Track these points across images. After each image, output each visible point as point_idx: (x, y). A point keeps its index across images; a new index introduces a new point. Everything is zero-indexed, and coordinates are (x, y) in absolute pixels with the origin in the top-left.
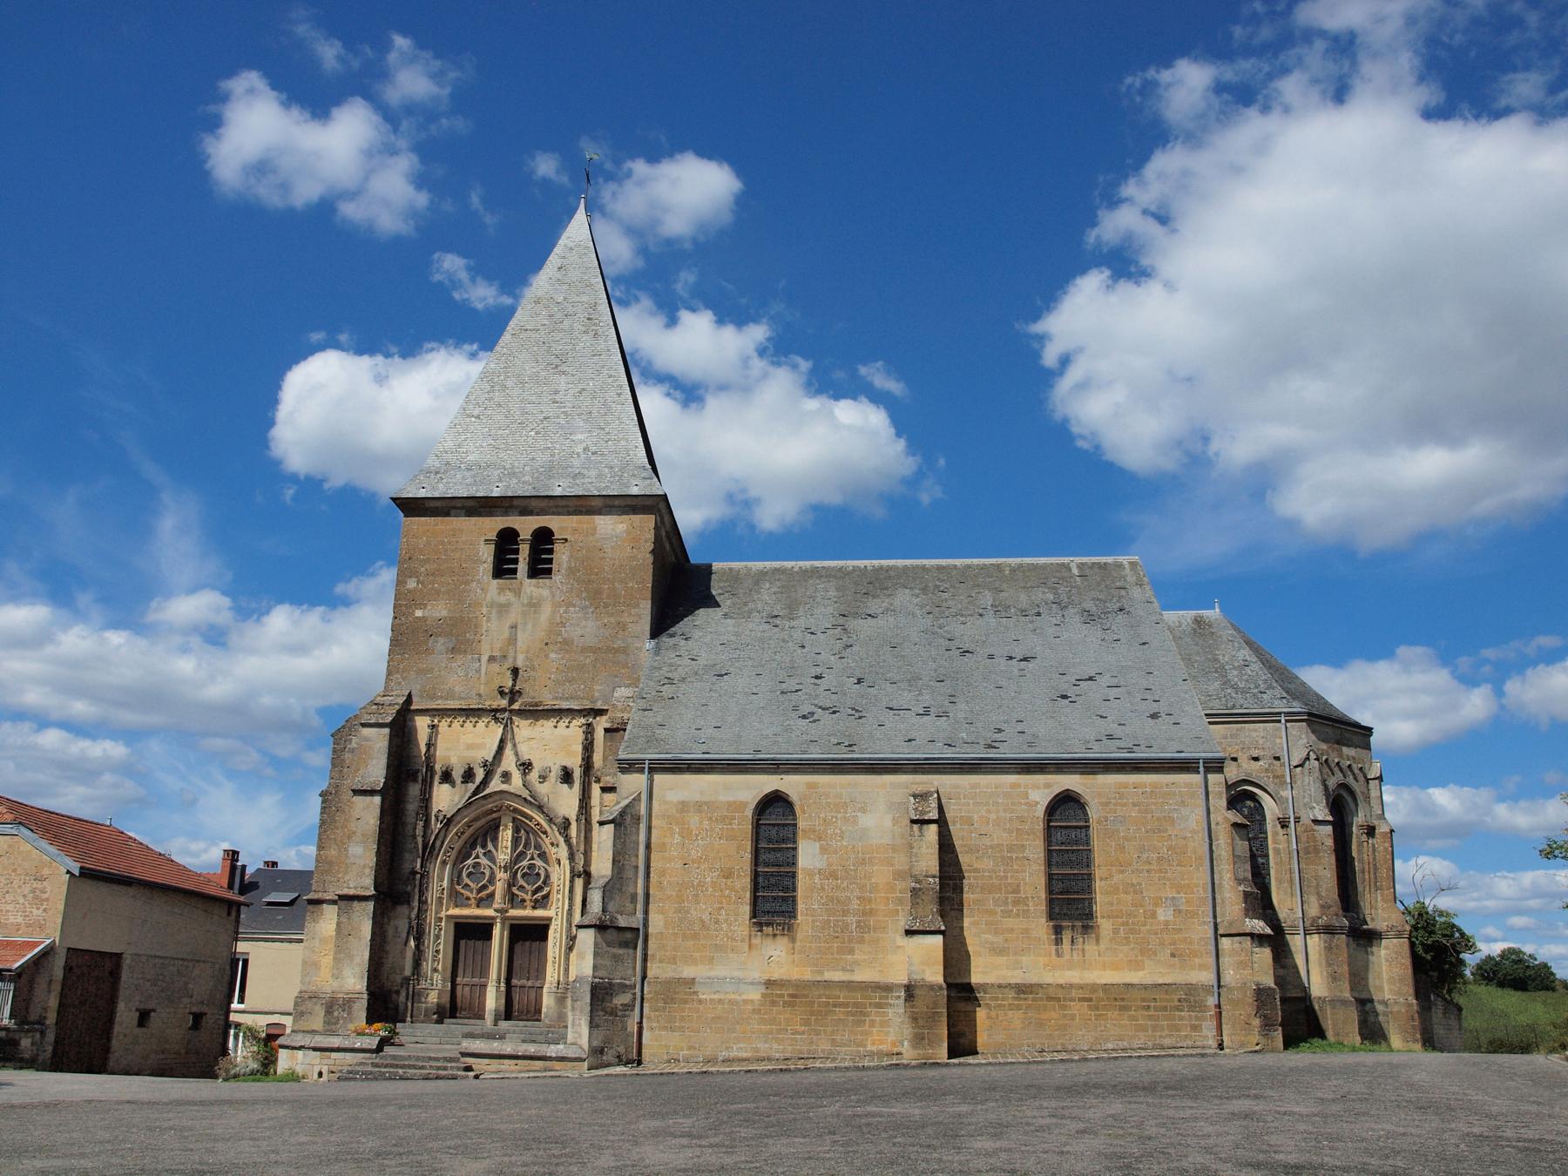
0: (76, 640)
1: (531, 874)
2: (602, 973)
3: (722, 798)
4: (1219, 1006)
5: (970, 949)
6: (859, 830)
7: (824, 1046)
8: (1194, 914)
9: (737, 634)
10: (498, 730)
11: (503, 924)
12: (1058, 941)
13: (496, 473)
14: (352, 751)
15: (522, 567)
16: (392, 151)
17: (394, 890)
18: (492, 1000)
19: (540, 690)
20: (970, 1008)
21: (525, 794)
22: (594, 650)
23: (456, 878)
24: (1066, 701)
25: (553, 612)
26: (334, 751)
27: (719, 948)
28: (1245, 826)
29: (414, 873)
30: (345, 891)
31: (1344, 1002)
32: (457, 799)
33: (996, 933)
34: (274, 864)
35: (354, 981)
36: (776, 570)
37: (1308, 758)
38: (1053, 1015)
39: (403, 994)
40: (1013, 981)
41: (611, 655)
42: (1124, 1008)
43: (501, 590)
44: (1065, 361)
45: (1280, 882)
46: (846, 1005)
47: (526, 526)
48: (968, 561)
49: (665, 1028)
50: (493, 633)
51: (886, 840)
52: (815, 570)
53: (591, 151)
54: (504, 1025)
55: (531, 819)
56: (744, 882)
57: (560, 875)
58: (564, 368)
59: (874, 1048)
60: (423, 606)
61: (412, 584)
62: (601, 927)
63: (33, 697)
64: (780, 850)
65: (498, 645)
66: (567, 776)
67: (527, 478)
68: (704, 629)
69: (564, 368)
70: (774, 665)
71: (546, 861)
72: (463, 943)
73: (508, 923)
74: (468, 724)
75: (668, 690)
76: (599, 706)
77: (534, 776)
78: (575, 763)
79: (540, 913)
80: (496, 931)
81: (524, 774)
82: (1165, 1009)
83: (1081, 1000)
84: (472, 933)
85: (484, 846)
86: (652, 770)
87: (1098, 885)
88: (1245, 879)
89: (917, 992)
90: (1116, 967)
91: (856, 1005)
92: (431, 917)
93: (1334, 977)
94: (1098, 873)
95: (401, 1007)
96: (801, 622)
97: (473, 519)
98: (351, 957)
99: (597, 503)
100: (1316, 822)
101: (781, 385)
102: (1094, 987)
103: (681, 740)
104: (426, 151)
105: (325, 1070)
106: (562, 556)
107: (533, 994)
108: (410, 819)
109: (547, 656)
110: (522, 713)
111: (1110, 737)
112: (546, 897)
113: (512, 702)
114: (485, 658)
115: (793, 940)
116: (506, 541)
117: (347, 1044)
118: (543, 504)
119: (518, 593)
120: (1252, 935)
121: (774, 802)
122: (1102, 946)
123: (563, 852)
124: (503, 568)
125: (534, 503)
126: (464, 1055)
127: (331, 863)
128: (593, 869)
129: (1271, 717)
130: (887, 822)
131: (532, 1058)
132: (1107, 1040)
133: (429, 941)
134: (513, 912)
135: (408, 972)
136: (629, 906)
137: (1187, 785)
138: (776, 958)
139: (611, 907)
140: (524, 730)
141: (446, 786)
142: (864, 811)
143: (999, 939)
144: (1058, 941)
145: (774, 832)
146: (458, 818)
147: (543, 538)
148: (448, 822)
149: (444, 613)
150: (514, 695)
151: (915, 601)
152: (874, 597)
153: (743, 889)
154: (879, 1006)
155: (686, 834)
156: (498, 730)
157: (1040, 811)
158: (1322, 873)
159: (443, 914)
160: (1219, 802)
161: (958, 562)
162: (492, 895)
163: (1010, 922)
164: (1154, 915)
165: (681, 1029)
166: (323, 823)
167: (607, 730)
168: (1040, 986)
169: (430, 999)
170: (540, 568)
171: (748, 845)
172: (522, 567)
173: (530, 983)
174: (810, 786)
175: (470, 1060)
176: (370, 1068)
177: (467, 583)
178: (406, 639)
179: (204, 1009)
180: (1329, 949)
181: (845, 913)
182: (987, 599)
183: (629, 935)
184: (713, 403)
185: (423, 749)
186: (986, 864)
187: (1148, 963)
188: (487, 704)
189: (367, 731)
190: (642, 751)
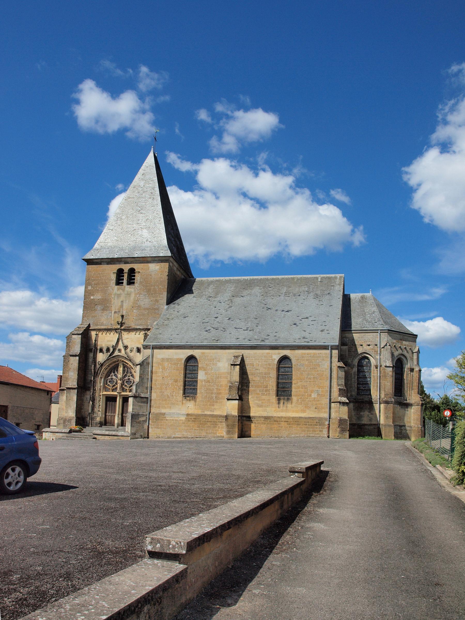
0: (43, 303)
3: (175, 357)
4: (329, 424)
5: (251, 405)
6: (218, 368)
7: (204, 434)
9: (195, 303)
10: (117, 336)
13: (117, 249)
15: (125, 281)
16: (143, 112)
17: (84, 386)
18: (117, 420)
19: (130, 322)
20: (249, 423)
21: (126, 356)
22: (148, 309)
24: (295, 326)
25: (135, 297)
26: (67, 343)
28: (344, 367)
29: (91, 381)
31: (390, 426)
33: (259, 400)
36: (217, 281)
37: (386, 345)
38: (276, 426)
39: (89, 418)
41: (153, 311)
42: (298, 424)
44: (419, 185)
45: (374, 386)
46: (211, 422)
47: (126, 267)
48: (283, 277)
49: (156, 428)
50: (115, 304)
51: (226, 371)
52: (230, 280)
53: (219, 108)
54: (120, 428)
55: (128, 364)
56: (181, 384)
58: (142, 211)
59: (219, 435)
60: (93, 295)
62: (135, 397)
63: (29, 324)
64: (193, 373)
65: (117, 308)
67: (127, 251)
68: (186, 300)
69: (142, 211)
70: (204, 313)
71: (133, 377)
72: (108, 403)
73: (121, 397)
74: (108, 334)
75: (166, 322)
76: (149, 327)
77: (128, 350)
82: (311, 425)
84: (111, 400)
85: (114, 373)
86: (153, 348)
89: (229, 418)
90: (297, 412)
91: (214, 422)
92: (97, 395)
93: (387, 417)
94: (294, 382)
96: (218, 299)
98: (71, 407)
99: (150, 259)
100: (386, 366)
101: (301, 201)
102: (289, 418)
103: (165, 340)
104: (155, 110)
106: (138, 278)
108: (90, 364)
109: (133, 311)
110: (124, 330)
111: (304, 338)
113: (121, 326)
114: (113, 312)
115: (195, 402)
116: (120, 272)
117: (60, 431)
118: (141, 259)
119: (124, 290)
120: (340, 402)
121: (191, 358)
122: (293, 405)
124: (119, 282)
125: (129, 260)
126: (94, 434)
129: (375, 331)
132: (292, 434)
133: (97, 402)
134: (123, 393)
135: (90, 411)
136: (145, 391)
137: (326, 354)
138: (190, 407)
139: (139, 391)
140: (125, 335)
141: (101, 354)
142: (219, 361)
143: (260, 402)
145: (191, 368)
146: (105, 364)
147: (132, 271)
148: (102, 365)
149: (100, 297)
150: (122, 324)
151: (260, 291)
152: (246, 290)
155: (164, 368)
156: (117, 336)
158: (386, 383)
159: (101, 394)
160: (335, 359)
161: (280, 277)
162: (117, 388)
163: (264, 397)
164: (310, 395)
165: (161, 428)
166: (64, 365)
168: (272, 417)
169: (97, 419)
170: (131, 282)
171: (182, 372)
172: (125, 281)
174: (203, 353)
175: (96, 436)
177: (107, 287)
178: (88, 306)
179: (40, 423)
180: (386, 408)
181: (212, 393)
182: (284, 290)
183: (145, 400)
184: (272, 209)
185: (94, 342)
186: (257, 379)
190: (151, 342)
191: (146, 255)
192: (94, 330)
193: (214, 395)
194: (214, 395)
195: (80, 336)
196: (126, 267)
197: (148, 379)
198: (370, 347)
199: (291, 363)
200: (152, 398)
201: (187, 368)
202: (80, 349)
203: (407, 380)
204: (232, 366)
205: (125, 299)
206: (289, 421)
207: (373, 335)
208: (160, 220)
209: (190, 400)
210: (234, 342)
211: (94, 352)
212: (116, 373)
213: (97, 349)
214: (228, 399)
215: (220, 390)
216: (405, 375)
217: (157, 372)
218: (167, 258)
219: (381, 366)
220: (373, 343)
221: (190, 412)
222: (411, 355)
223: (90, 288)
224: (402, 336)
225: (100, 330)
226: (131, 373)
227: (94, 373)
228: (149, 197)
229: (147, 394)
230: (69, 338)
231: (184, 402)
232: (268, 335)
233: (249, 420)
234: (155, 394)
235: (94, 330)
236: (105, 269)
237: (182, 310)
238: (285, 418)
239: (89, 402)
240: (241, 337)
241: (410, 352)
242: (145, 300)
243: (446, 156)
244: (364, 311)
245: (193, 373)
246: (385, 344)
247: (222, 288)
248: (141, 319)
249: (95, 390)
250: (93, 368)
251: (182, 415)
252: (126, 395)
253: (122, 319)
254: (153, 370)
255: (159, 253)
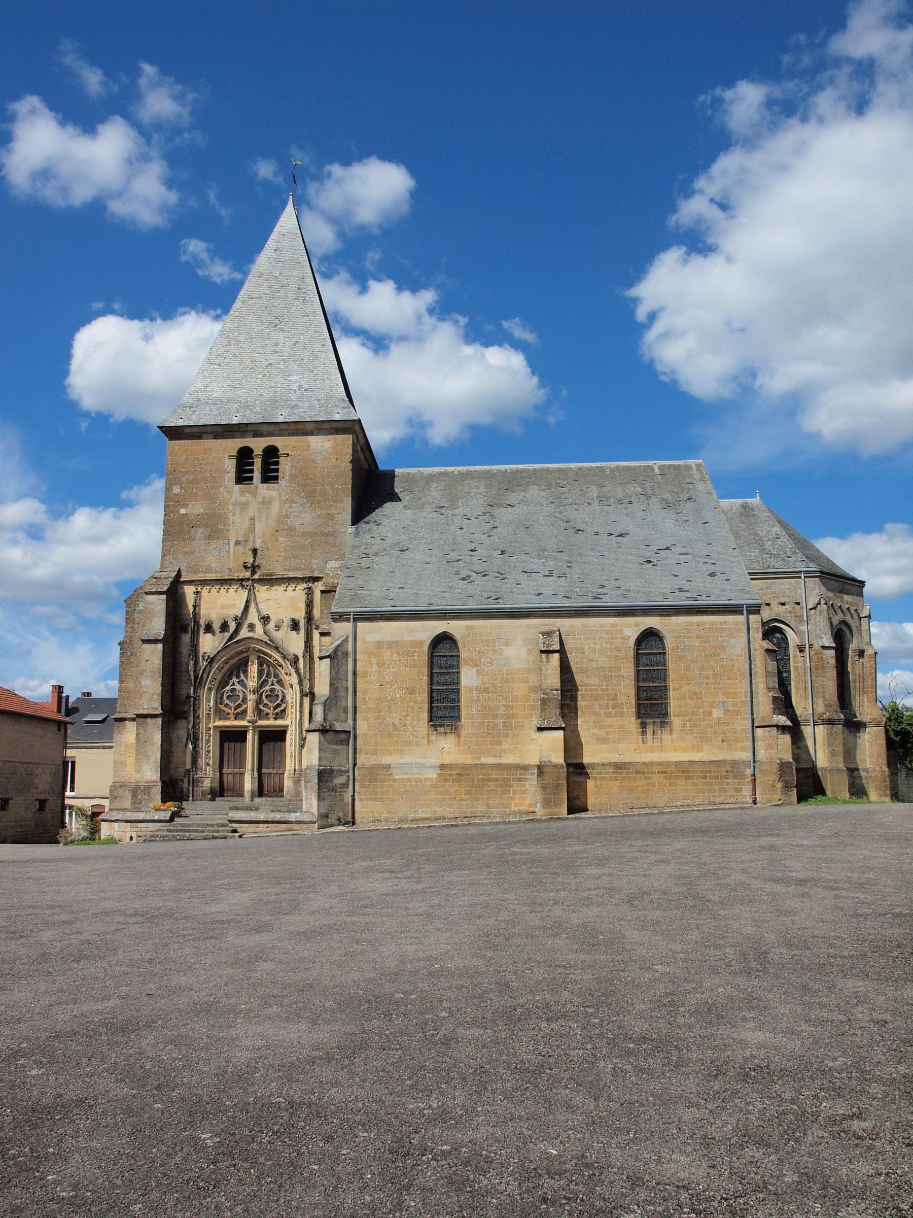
1: (272, 695)
2: (325, 763)
3: (406, 638)
4: (754, 775)
5: (583, 739)
6: (504, 659)
7: (481, 808)
8: (738, 713)
9: (414, 521)
10: (244, 594)
11: (254, 731)
12: (644, 733)
13: (234, 406)
14: (140, 612)
15: (257, 475)
16: (145, 158)
17: (175, 709)
18: (249, 784)
19: (272, 565)
21: (266, 639)
23: (219, 700)
24: (650, 565)
25: (281, 508)
26: (127, 613)
27: (408, 743)
29: (189, 697)
30: (141, 712)
31: (839, 771)
32: (217, 643)
34: (89, 694)
35: (151, 773)
36: (441, 474)
37: (819, 603)
39: (186, 780)
40: (612, 761)
41: (323, 538)
42: (688, 778)
43: (242, 493)
45: (797, 689)
46: (497, 780)
47: (258, 445)
48: (580, 465)
49: (371, 799)
50: (237, 525)
51: (523, 665)
53: (299, 158)
54: (258, 800)
55: (270, 656)
56: (424, 697)
57: (293, 695)
59: (516, 809)
60: (186, 506)
61: (176, 490)
64: (448, 673)
65: (241, 532)
66: (295, 626)
67: (257, 409)
69: (281, 326)
70: (441, 542)
74: (222, 590)
75: (365, 562)
76: (316, 574)
77: (271, 626)
78: (301, 616)
79: (279, 722)
80: (250, 736)
81: (265, 625)
82: (717, 777)
83: (658, 772)
84: (232, 738)
85: (238, 676)
87: (672, 694)
88: (774, 688)
89: (545, 770)
90: (683, 750)
91: (504, 780)
92: (203, 727)
93: (833, 754)
94: (672, 685)
95: (185, 790)
96: (460, 511)
97: (220, 441)
99: (310, 427)
100: (823, 647)
101: (445, 335)
102: (668, 764)
105: (134, 835)
106: (285, 466)
107: (277, 779)
108: (184, 659)
110: (261, 581)
112: (284, 711)
113: (253, 573)
114: (232, 543)
115: (459, 736)
116: (244, 456)
117: (148, 817)
118: (272, 428)
119: (254, 494)
120: (777, 726)
121: (443, 640)
122: (674, 736)
123: (294, 679)
124: (243, 476)
125: (263, 428)
126: (231, 821)
127: (129, 692)
128: (316, 690)
129: (795, 575)
130: (524, 652)
131: (278, 822)
132: (677, 799)
133: (202, 744)
134: (261, 723)
135: (188, 766)
136: (343, 716)
137: (737, 623)
138: (447, 749)
139: (330, 717)
140: (262, 592)
141: (209, 635)
142: (507, 645)
143: (602, 733)
144: (644, 733)
146: (218, 658)
147: (271, 453)
148: (212, 660)
149: (201, 510)
151: (542, 494)
152: (513, 492)
153: (422, 702)
154: (520, 780)
155: (381, 664)
156: (244, 594)
157: (631, 643)
159: (211, 725)
160: (757, 635)
162: (245, 711)
163: (610, 721)
164: (710, 714)
165: (382, 799)
167: (322, 592)
169: (205, 784)
170: (270, 475)
171: (425, 671)
172: (257, 475)
173: (274, 771)
174: (470, 628)
175: (235, 825)
176: (166, 833)
177: (217, 488)
178: (175, 530)
180: (830, 734)
181: (495, 716)
183: (343, 736)
184: (396, 350)
185: (191, 609)
186: (593, 681)
187: (706, 747)
188: (236, 576)
189: (150, 598)
191: (303, 417)
192: (191, 582)
193: (499, 721)
194: (499, 721)
195: (164, 597)
196: (258, 445)
197: (347, 688)
198: (787, 607)
199: (663, 644)
200: (358, 732)
201: (435, 661)
202: (164, 626)
203: (854, 674)
204: (544, 655)
205: (258, 514)
206: (668, 770)
207: (789, 583)
208: (323, 345)
209: (446, 733)
210: (534, 603)
211: (193, 632)
212: (242, 677)
213: (197, 623)
214: (540, 729)
215: (512, 708)
216: (849, 664)
217: (366, 672)
218: (349, 425)
219: (811, 646)
220: (792, 600)
221: (447, 760)
222: (857, 624)
223: (176, 490)
224: (841, 584)
225: (204, 583)
226: (276, 676)
227: (196, 677)
228: (295, 296)
229: (346, 725)
230: (131, 603)
231: (433, 738)
232: (603, 586)
233: (582, 773)
234: (365, 723)
235: (191, 582)
236: (211, 449)
237: (390, 535)
238: (660, 764)
239: (186, 746)
240: (547, 592)
241: (856, 616)
242: (303, 515)
243: (697, 261)
244: (756, 534)
245: (448, 673)
246: (817, 601)
247: (459, 488)
248: (296, 557)
249: (198, 717)
250: (191, 668)
251: (431, 767)
252: (241, 727)
253: (255, 558)
254: (358, 669)
255: (331, 413)
